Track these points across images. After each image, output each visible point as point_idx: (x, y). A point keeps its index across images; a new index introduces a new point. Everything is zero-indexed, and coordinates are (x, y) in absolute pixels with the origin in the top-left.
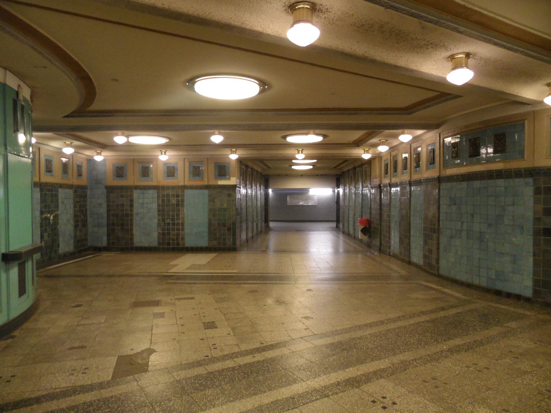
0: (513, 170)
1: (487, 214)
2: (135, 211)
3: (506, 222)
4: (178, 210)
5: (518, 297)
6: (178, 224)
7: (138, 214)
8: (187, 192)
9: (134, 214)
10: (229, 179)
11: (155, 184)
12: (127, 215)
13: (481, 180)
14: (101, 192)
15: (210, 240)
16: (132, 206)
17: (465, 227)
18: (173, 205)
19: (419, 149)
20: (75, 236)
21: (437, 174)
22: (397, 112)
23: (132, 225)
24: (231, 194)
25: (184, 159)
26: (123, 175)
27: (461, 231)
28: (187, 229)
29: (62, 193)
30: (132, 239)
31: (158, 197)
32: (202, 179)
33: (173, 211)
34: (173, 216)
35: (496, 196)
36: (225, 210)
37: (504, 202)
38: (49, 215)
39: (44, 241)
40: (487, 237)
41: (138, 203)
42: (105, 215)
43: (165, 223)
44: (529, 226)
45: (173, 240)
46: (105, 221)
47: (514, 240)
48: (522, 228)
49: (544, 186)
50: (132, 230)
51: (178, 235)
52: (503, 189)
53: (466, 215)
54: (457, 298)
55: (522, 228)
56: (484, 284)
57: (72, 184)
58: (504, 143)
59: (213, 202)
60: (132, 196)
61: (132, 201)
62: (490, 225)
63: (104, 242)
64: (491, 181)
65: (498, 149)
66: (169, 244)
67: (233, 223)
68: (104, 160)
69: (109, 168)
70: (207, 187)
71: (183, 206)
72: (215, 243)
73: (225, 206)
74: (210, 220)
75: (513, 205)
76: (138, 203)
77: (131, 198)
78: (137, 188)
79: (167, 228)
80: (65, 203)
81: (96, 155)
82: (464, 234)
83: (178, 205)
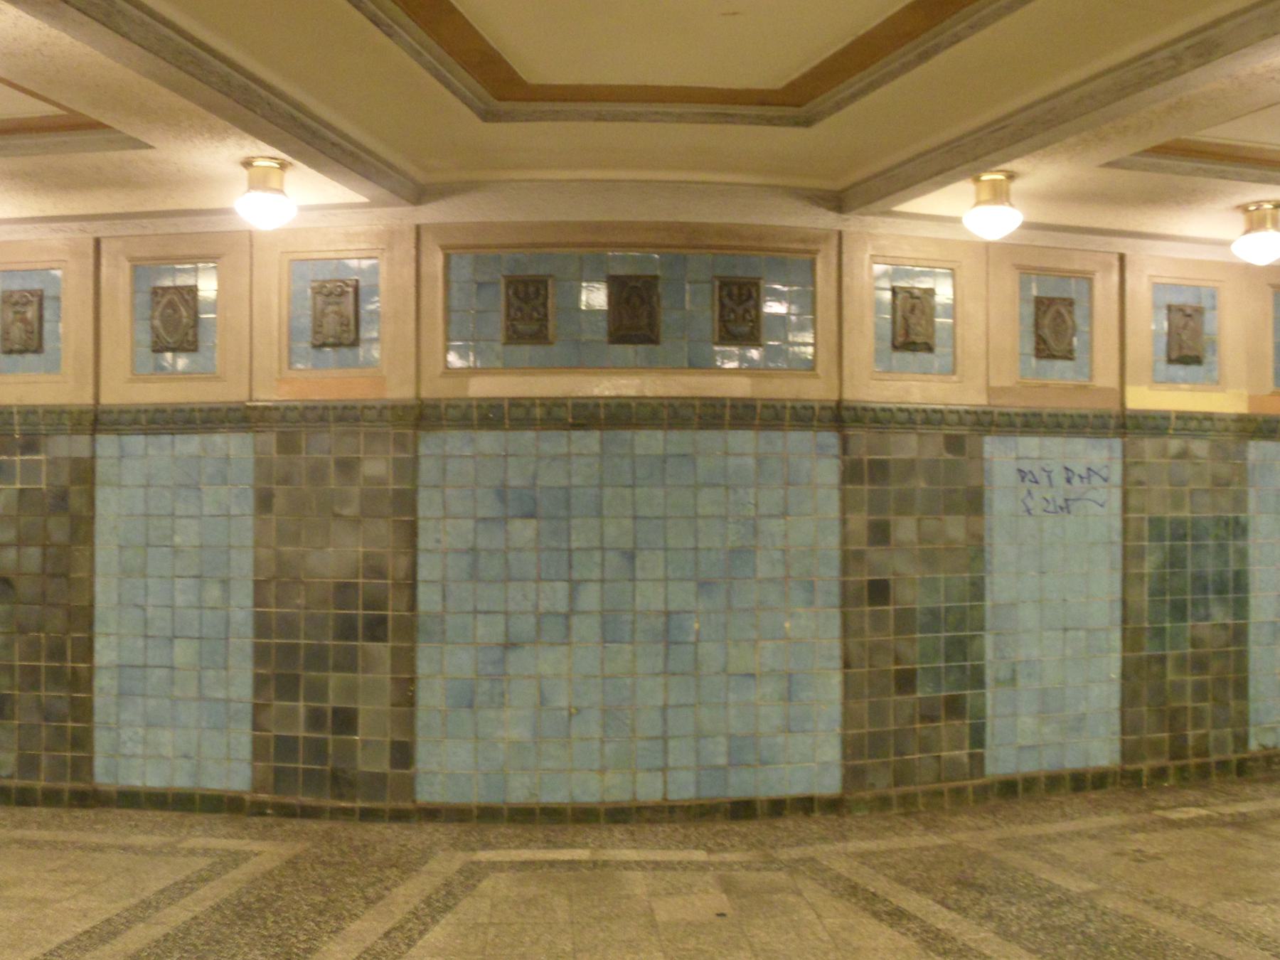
0: (474, 403)
1: (696, 549)
3: (763, 570)
5: (806, 805)
13: (671, 427)
17: (590, 597)
19: (58, 273)
21: (835, 397)
22: (754, 110)
27: (567, 616)
35: (727, 488)
37: (756, 505)
40: (696, 626)
44: (829, 574)
47: (787, 625)
48: (810, 587)
52: (750, 461)
53: (597, 556)
54: (1057, 862)
55: (810, 587)
56: (683, 789)
57: (118, 938)
58: (541, 310)
62: (704, 586)
64: (775, 435)
65: (521, 327)
75: (784, 514)
82: (586, 627)
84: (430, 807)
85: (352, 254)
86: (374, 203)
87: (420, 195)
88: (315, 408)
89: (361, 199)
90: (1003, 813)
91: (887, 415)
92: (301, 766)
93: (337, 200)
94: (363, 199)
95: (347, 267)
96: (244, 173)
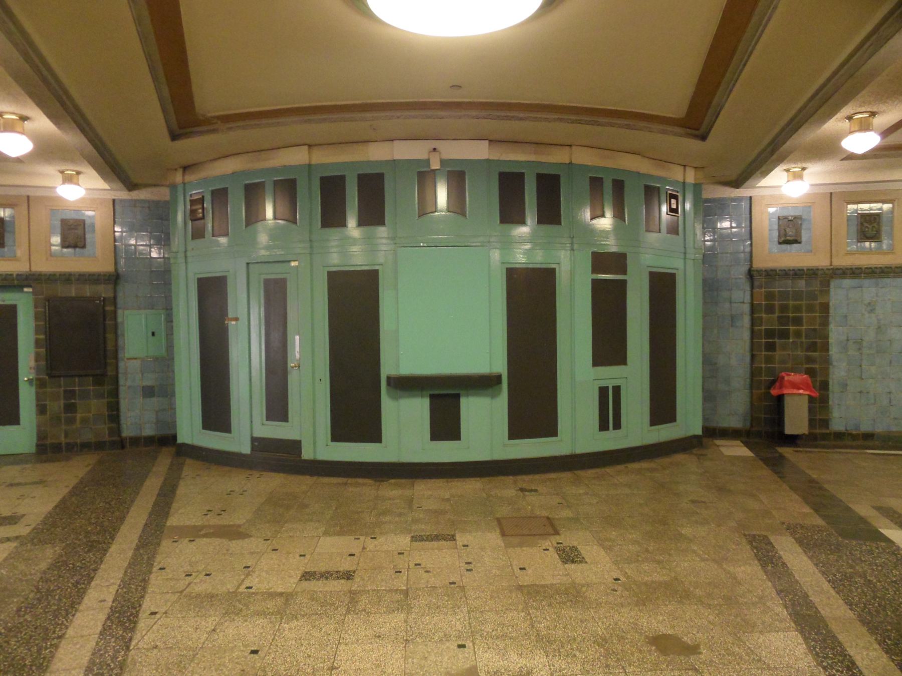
26: (798, 239)
84: (227, 468)
85: (84, 209)
86: (111, 190)
87: (131, 186)
88: (65, 275)
89: (107, 186)
90: (423, 486)
91: (774, 272)
92: (763, 378)
93: (95, 187)
94: (109, 188)
95: (84, 214)
96: (60, 175)
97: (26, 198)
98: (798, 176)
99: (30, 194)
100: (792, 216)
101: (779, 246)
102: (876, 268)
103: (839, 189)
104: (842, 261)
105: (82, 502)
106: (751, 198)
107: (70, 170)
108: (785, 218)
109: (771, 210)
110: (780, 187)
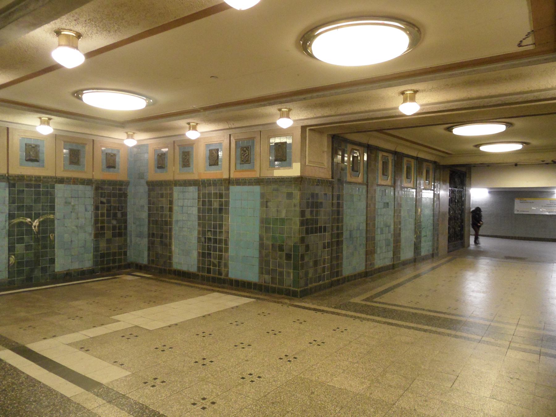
2: (174, 218)
4: (221, 219)
6: (221, 241)
7: (177, 221)
8: (234, 189)
9: (173, 221)
10: (290, 165)
11: (195, 177)
12: (166, 223)
14: (143, 189)
15: (261, 272)
16: (171, 209)
18: (215, 209)
20: (96, 249)
23: (171, 238)
24: (292, 193)
25: (230, 135)
26: (163, 166)
28: (232, 252)
29: (60, 191)
30: (170, 258)
31: (199, 198)
32: (252, 169)
33: (215, 220)
34: (215, 227)
36: (283, 221)
38: (29, 220)
39: (14, 255)
41: (178, 206)
42: (147, 220)
43: (205, 238)
45: (214, 265)
46: (145, 229)
49: (104, 218)
50: (170, 244)
51: (220, 257)
59: (267, 207)
60: (171, 195)
61: (171, 202)
63: (144, 261)
66: (209, 271)
67: (294, 246)
68: (137, 147)
69: (149, 157)
70: (259, 181)
71: (227, 212)
72: (267, 277)
73: (283, 215)
74: (261, 238)
76: (178, 206)
77: (171, 199)
78: (177, 183)
79: (208, 246)
80: (73, 204)
81: (127, 139)
83: (221, 210)
93: (64, 129)
97: (92, 141)
98: (47, 123)
99: (95, 139)
100: (34, 145)
101: (26, 162)
102: (16, 176)
103: (62, 133)
104: (61, 174)
105: (139, 396)
106: (8, 129)
107: (45, 117)
108: (30, 145)
109: (103, 148)
110: (36, 126)
